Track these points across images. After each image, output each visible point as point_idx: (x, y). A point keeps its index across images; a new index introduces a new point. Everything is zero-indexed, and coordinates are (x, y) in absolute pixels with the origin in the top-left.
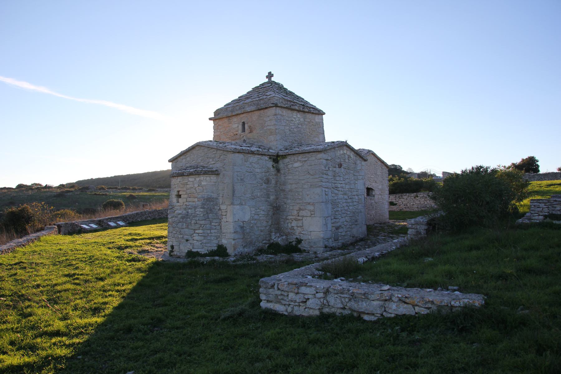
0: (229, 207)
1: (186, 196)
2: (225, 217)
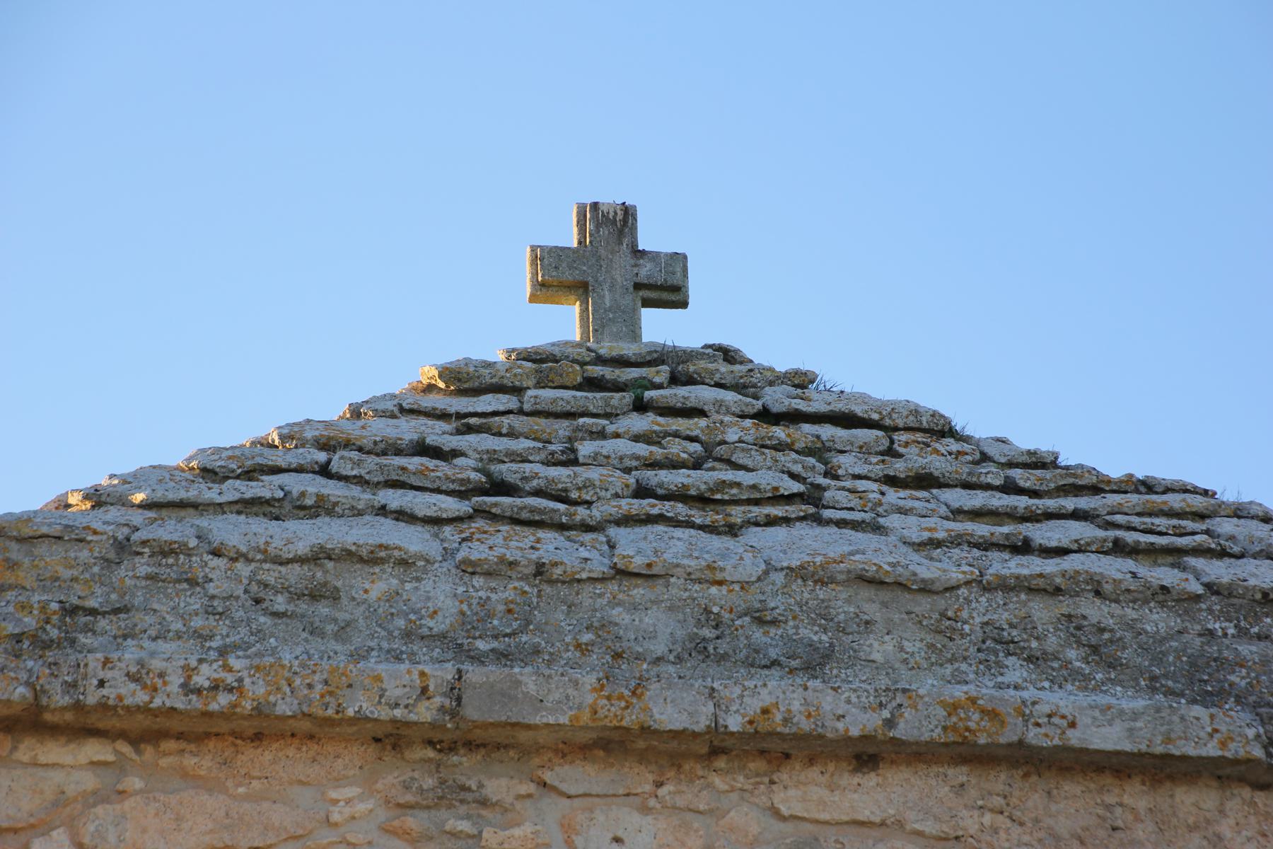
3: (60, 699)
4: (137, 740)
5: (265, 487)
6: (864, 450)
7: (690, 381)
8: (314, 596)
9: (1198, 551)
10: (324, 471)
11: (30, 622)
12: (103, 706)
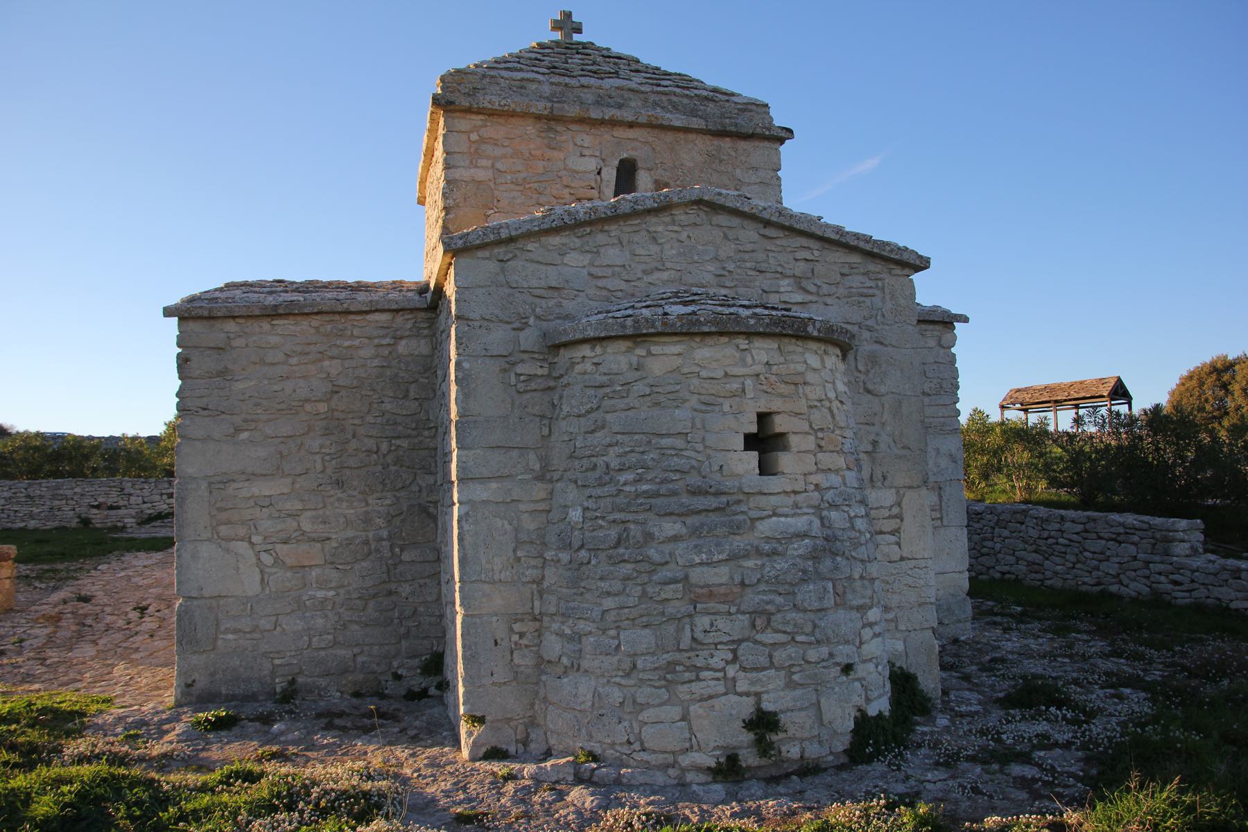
0: (909, 494)
1: (810, 443)
2: (893, 539)
5: (508, 65)
8: (521, 88)
10: (519, 62)
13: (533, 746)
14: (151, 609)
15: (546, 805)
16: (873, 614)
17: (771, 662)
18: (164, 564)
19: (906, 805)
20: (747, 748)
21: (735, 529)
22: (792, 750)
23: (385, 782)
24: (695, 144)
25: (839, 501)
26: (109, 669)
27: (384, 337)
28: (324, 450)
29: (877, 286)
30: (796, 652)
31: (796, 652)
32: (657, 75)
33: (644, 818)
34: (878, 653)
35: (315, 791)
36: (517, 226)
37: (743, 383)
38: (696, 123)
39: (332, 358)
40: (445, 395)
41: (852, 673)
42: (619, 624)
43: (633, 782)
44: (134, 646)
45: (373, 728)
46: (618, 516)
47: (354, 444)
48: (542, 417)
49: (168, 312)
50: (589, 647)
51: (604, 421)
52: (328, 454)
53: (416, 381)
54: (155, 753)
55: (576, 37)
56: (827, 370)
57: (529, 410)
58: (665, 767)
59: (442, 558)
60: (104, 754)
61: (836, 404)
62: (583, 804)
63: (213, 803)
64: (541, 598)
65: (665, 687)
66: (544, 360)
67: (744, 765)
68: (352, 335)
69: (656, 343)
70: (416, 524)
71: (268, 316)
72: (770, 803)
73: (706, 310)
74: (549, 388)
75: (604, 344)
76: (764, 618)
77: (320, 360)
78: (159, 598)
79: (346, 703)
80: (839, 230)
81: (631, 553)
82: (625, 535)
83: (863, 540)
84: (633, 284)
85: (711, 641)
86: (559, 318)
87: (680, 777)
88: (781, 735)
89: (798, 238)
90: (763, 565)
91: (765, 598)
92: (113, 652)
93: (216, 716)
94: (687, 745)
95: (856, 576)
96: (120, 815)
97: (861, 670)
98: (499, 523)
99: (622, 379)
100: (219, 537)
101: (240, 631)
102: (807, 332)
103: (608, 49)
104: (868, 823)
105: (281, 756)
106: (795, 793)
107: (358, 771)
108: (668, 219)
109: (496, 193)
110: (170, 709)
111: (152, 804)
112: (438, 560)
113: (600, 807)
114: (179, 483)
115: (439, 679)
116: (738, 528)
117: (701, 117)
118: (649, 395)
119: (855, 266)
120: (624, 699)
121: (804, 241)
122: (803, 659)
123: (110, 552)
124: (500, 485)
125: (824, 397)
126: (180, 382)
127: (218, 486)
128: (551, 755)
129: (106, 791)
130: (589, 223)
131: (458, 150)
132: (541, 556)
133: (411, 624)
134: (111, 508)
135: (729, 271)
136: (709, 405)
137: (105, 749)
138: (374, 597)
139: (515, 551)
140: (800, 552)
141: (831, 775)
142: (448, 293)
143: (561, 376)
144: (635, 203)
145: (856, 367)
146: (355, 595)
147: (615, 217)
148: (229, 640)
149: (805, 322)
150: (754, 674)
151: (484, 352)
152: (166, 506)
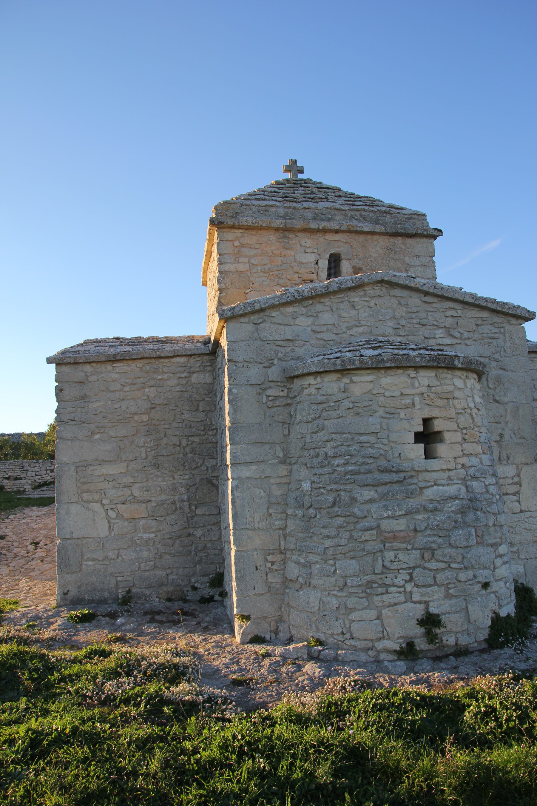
2: (515, 498)
3: (237, 224)
4: (246, 229)
6: (331, 192)
7: (306, 183)
8: (266, 211)
9: (376, 206)
10: (264, 195)
11: (231, 214)
12: (242, 225)
13: (281, 634)
14: (41, 544)
15: (290, 674)
16: (503, 549)
17: (435, 581)
18: (49, 515)
19: (527, 678)
20: (421, 637)
21: (410, 495)
22: (450, 639)
23: (187, 658)
24: (379, 242)
25: (478, 475)
26: (17, 582)
27: (182, 372)
28: (146, 445)
29: (500, 332)
30: (451, 575)
31: (451, 575)
32: (352, 198)
33: (353, 684)
34: (506, 575)
35: (144, 663)
36: (265, 301)
37: (413, 399)
38: (379, 228)
39: (150, 386)
40: (222, 409)
41: (489, 588)
42: (336, 556)
43: (345, 659)
44: (32, 567)
45: (179, 622)
46: (333, 487)
47: (165, 440)
48: (284, 423)
49: (49, 361)
50: (316, 571)
51: (323, 425)
52: (149, 447)
53: (203, 400)
54: (45, 637)
55: (300, 176)
56: (468, 389)
57: (276, 418)
58: (367, 650)
59: (221, 512)
60: (15, 637)
61: (474, 411)
62: (314, 673)
63: (81, 671)
64: (285, 539)
65: (365, 597)
66: (284, 386)
67: (418, 649)
68: (163, 371)
69: (356, 375)
70: (205, 491)
71: (110, 361)
72: (436, 675)
73: (388, 352)
74: (288, 404)
75: (323, 375)
76: (430, 552)
77: (144, 388)
78: (46, 536)
79: (162, 605)
80: (474, 296)
81: (342, 511)
82: (338, 499)
83: (494, 500)
84: (340, 336)
85: (395, 567)
86: (293, 359)
87: (376, 657)
88: (442, 630)
89: (447, 303)
90: (429, 518)
91: (430, 539)
92: (19, 571)
93: (82, 614)
94: (381, 635)
95: (491, 524)
96: (25, 677)
97: (495, 586)
98: (257, 491)
99: (334, 398)
100: (82, 500)
101: (96, 559)
102: (454, 365)
103: (321, 183)
104: (501, 690)
105: (121, 640)
106: (452, 668)
107: (170, 651)
108: (362, 293)
109: (252, 279)
110: (54, 609)
111: (44, 670)
112: (219, 513)
113: (324, 676)
114: (58, 467)
115: (220, 589)
116: (412, 494)
117: (382, 224)
118: (352, 408)
119: (485, 319)
120: (339, 605)
121: (451, 304)
122: (456, 579)
123: (16, 507)
124: (257, 467)
125: (467, 407)
126: (57, 404)
127: (81, 468)
128: (293, 641)
129: (16, 662)
130: (312, 298)
131: (226, 253)
132: (285, 512)
133: (202, 554)
134: (16, 479)
135: (403, 326)
136: (391, 414)
137: (15, 634)
138: (179, 538)
139: (268, 509)
140: (453, 509)
141: (476, 656)
142: (222, 345)
143: (296, 396)
144: (340, 284)
145: (488, 385)
146: (167, 536)
147: (328, 293)
148: (90, 565)
149: (452, 358)
150: (424, 589)
151: (246, 383)
152: (49, 478)
